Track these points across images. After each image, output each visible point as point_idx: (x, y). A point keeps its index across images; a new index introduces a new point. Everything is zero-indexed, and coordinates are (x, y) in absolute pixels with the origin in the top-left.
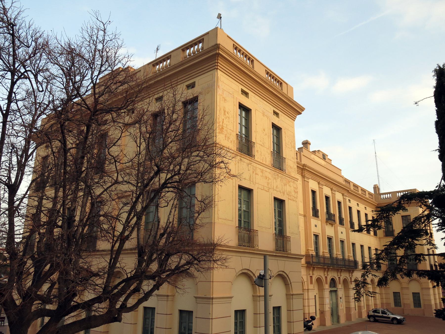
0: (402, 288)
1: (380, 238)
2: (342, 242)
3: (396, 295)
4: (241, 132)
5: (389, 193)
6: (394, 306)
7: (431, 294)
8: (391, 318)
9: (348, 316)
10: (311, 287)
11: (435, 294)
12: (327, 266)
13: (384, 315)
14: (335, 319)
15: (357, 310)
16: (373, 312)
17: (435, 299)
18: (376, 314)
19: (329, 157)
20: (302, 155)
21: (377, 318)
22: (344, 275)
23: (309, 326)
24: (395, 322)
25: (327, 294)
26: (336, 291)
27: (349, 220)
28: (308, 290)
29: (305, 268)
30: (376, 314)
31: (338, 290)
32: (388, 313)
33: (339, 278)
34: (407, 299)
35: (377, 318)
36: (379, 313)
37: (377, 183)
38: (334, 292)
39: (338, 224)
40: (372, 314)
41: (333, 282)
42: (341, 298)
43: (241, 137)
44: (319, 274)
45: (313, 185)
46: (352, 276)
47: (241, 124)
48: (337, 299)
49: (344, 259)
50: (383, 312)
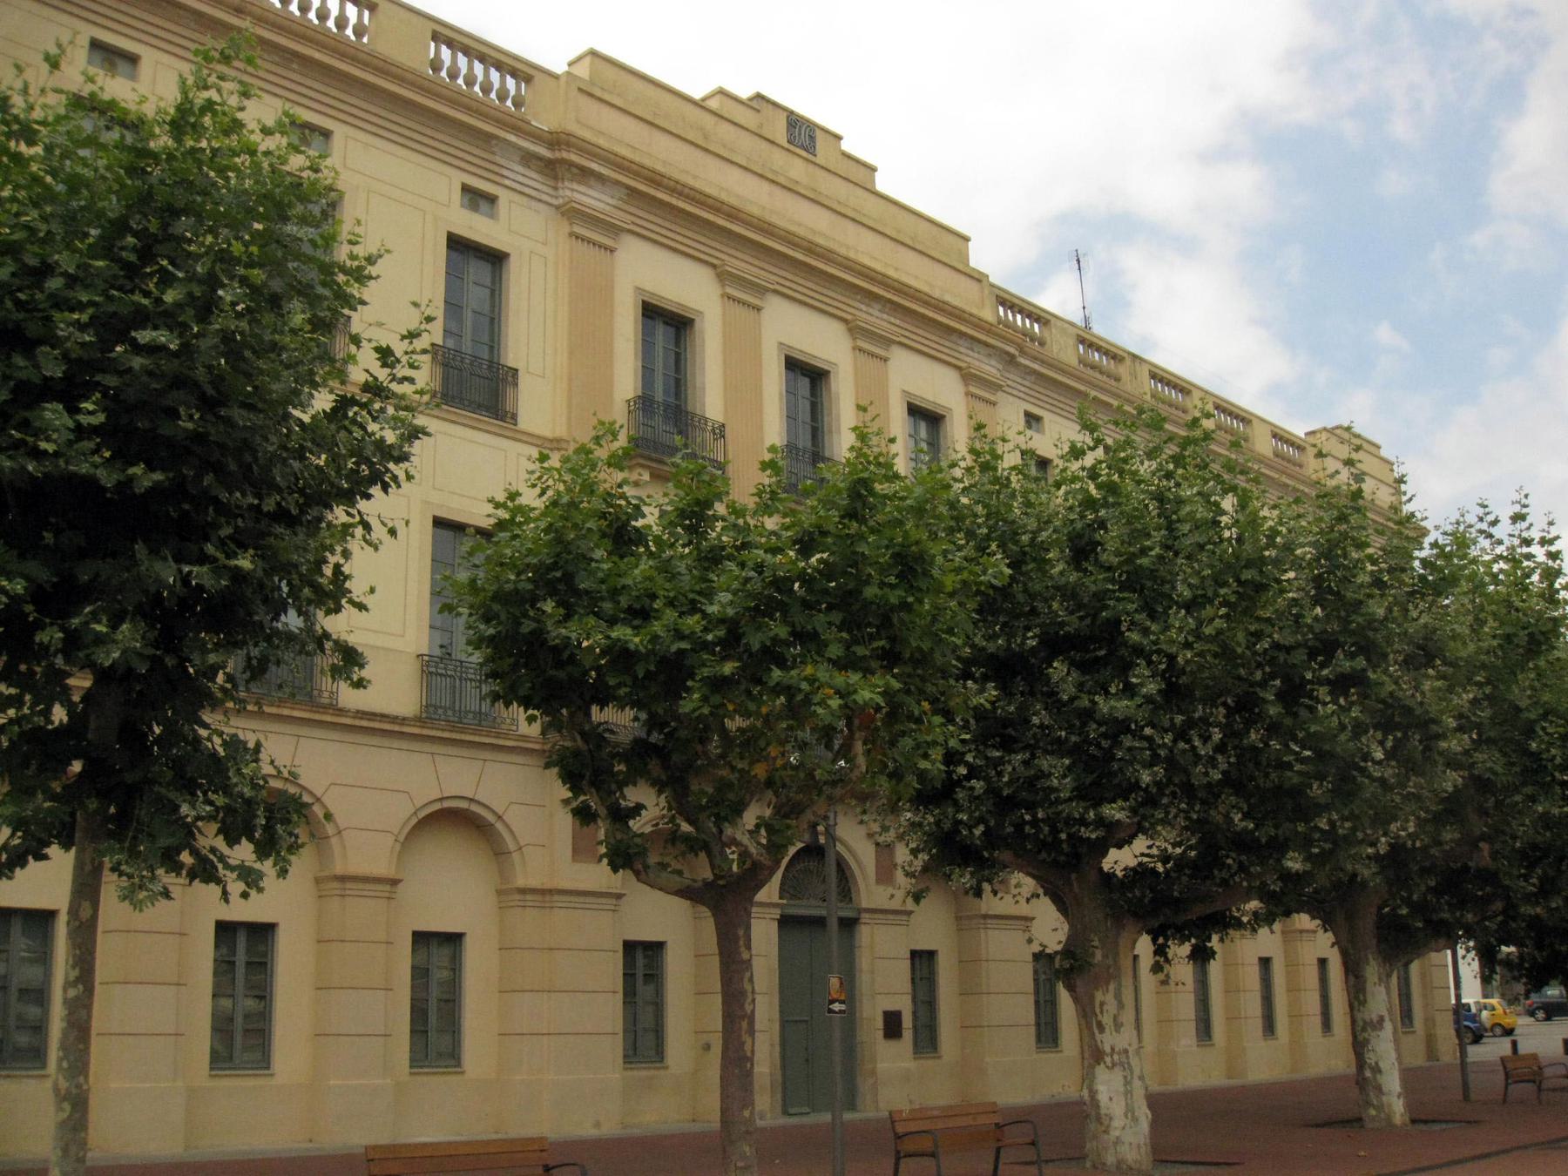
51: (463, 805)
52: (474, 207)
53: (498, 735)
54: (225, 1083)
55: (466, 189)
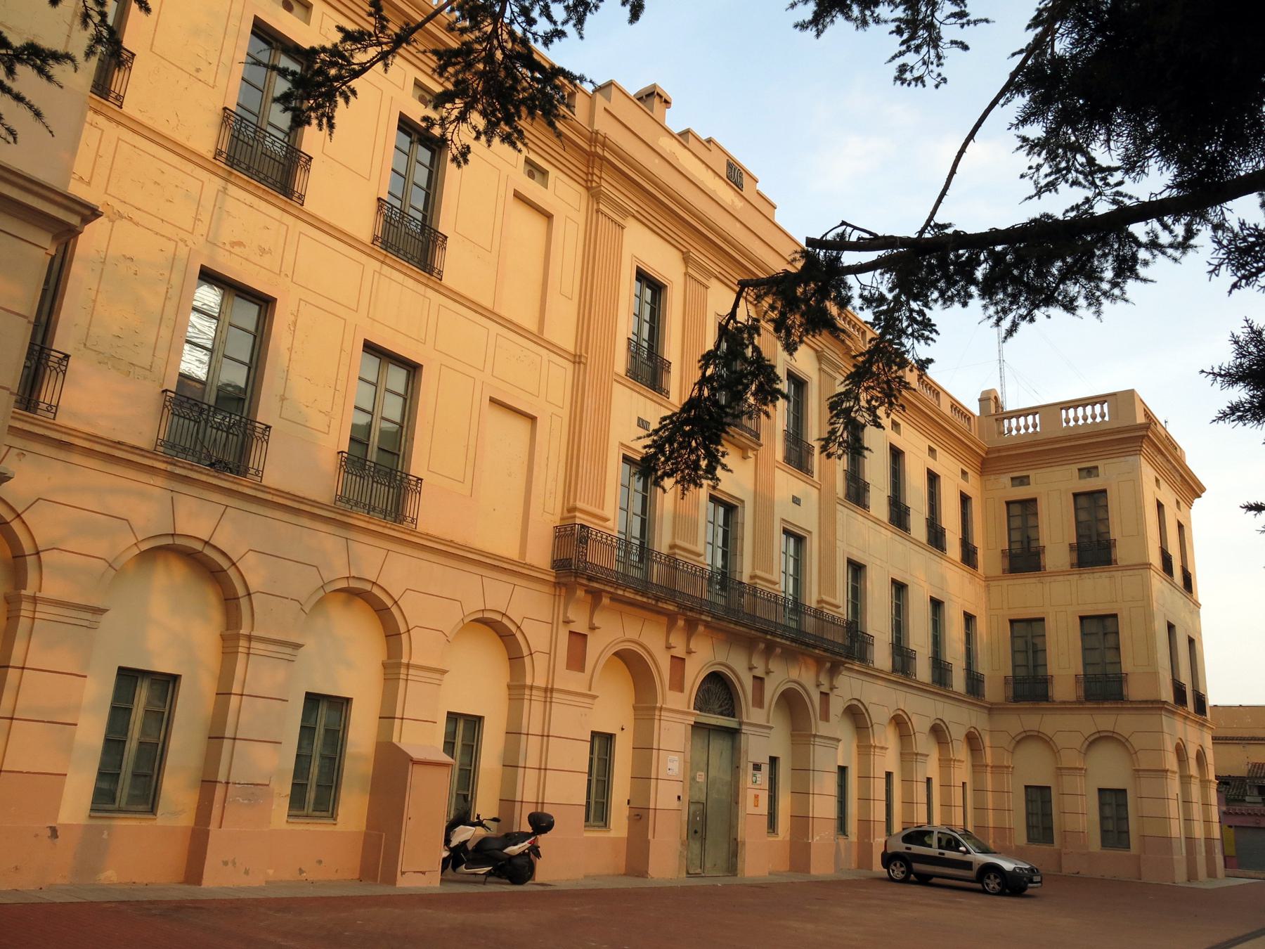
0: (1060, 771)
1: (987, 579)
3: (1039, 798)
4: (638, 334)
5: (1033, 411)
7: (1172, 795)
8: (976, 868)
9: (800, 851)
10: (568, 680)
12: (679, 606)
13: (949, 854)
17: (1188, 820)
18: (917, 849)
19: (759, 187)
21: (917, 867)
23: (511, 858)
24: (993, 884)
26: (733, 734)
30: (917, 849)
31: (745, 729)
32: (966, 845)
34: (1079, 814)
35: (917, 867)
36: (930, 846)
37: (993, 384)
39: (779, 454)
40: (900, 847)
41: (718, 690)
43: (638, 344)
47: (638, 316)
48: (735, 768)
49: (798, 607)
53: (911, 680)
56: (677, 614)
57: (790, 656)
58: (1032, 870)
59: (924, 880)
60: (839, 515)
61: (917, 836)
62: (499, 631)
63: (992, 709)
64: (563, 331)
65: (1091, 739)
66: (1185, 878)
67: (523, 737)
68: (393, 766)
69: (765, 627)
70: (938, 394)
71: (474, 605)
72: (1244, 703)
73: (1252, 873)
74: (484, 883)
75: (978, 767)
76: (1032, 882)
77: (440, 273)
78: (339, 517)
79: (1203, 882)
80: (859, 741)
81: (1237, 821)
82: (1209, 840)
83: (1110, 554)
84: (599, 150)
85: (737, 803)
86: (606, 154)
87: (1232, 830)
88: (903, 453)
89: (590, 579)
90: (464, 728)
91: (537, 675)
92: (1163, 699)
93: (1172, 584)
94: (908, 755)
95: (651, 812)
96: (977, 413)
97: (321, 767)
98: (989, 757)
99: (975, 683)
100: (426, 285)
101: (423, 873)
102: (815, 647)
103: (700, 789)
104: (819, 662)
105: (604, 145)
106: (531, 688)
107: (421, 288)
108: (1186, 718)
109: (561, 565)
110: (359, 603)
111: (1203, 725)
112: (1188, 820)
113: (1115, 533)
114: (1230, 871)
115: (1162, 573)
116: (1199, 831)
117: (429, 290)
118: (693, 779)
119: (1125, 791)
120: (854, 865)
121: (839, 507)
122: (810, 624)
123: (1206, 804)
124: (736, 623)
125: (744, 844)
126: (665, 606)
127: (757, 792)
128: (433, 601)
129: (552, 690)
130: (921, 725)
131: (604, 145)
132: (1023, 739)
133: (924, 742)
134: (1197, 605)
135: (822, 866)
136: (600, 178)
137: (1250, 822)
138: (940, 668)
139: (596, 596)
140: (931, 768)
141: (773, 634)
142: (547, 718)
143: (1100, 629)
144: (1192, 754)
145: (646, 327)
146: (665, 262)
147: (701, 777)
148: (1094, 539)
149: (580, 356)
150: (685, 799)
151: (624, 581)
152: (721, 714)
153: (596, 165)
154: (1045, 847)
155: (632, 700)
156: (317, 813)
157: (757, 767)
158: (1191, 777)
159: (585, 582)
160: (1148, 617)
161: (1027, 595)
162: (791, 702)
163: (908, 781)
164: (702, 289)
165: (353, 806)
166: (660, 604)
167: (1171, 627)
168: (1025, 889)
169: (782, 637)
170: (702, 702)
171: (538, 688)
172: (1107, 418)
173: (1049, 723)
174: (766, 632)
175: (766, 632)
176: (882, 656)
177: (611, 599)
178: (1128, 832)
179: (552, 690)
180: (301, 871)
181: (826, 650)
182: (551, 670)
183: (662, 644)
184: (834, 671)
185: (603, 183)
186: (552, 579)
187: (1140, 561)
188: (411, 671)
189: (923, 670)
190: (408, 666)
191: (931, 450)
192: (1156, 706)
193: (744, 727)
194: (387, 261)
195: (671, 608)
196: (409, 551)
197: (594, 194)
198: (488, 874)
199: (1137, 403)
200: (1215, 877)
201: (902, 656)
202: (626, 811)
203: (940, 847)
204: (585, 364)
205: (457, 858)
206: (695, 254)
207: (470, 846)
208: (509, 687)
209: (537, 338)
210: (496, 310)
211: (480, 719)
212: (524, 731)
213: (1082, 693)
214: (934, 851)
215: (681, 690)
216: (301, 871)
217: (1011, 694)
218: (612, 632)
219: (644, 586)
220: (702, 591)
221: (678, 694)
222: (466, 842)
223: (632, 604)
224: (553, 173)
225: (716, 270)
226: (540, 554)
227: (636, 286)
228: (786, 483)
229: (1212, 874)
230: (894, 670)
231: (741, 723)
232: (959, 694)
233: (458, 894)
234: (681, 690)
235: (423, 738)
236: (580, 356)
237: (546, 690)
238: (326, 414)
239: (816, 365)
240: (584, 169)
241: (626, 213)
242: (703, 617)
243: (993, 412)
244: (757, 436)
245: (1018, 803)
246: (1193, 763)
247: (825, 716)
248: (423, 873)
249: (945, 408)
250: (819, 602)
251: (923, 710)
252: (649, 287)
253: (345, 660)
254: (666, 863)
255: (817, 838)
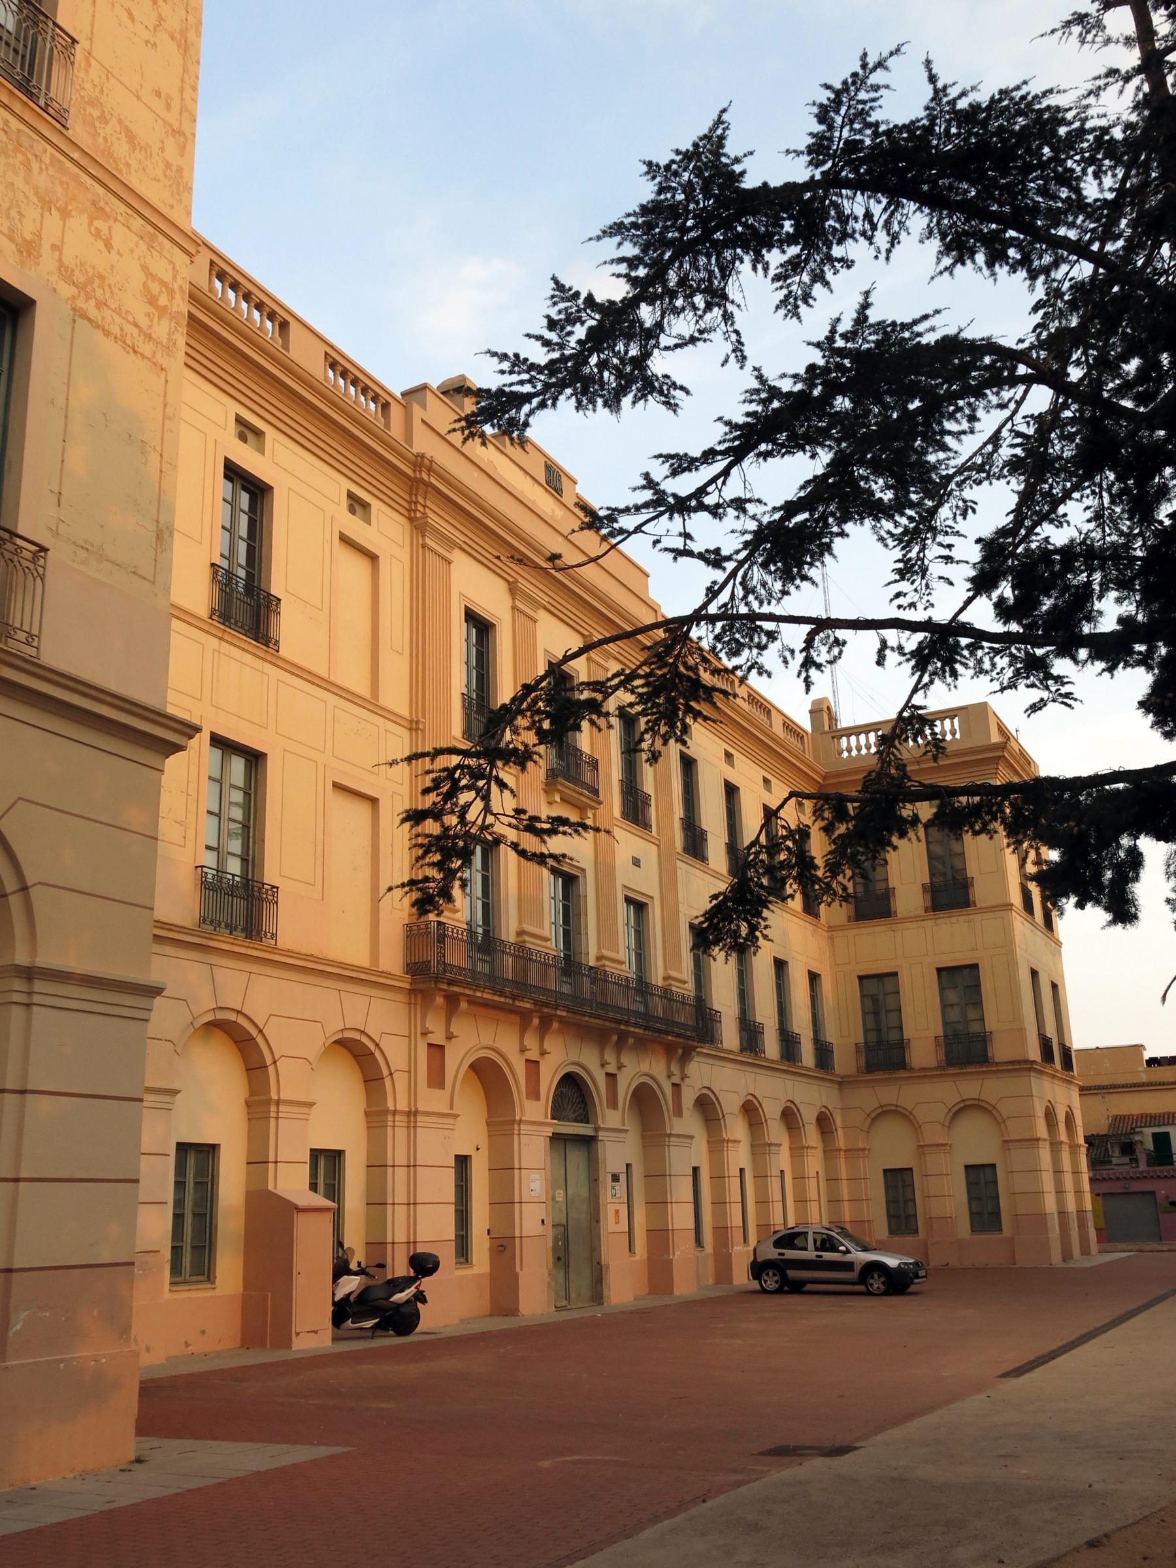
1: (831, 929)
2: (638, 907)
3: (898, 1182)
4: (230, 557)
6: (886, 1233)
8: (858, 1268)
9: (659, 1270)
10: (431, 1100)
11: (1058, 1172)
12: (536, 1002)
13: (828, 1256)
14: (581, 1282)
15: (709, 1248)
16: (778, 1244)
17: (1060, 1192)
18: (791, 1254)
19: (579, 489)
20: (417, 422)
21: (792, 1274)
22: (641, 1067)
23: (398, 1306)
24: (877, 1284)
25: (532, 1148)
26: (588, 1142)
27: (678, 811)
28: (412, 1114)
29: (402, 997)
30: (791, 1254)
33: (611, 1076)
34: (945, 1197)
35: (792, 1274)
36: (806, 1249)
38: (576, 1144)
40: (772, 1253)
41: (573, 1095)
42: (615, 1178)
43: (229, 573)
44: (487, 1040)
45: (476, 584)
46: (684, 1077)
47: (231, 530)
48: (594, 1181)
49: (642, 987)
50: (827, 1244)
51: (232, 1017)
52: (243, 438)
53: (718, 1049)
54: (984, 1237)
55: (240, 421)
56: (531, 1011)
57: (642, 1045)
58: (916, 1264)
59: (796, 1288)
60: (679, 872)
61: (788, 1240)
62: (356, 1052)
63: (842, 1084)
64: (395, 696)
65: (954, 1110)
66: (1060, 1259)
67: (390, 1170)
68: (271, 1218)
69: (618, 1016)
70: (769, 712)
71: (334, 1027)
72: (1101, 1045)
73: (1124, 1246)
74: (373, 1338)
75: (830, 1152)
76: (917, 1277)
77: (277, 643)
78: (204, 942)
79: (1079, 1261)
80: (709, 1135)
81: (1105, 1188)
82: (1081, 1212)
83: (967, 894)
84: (425, 477)
85: (598, 1221)
86: (433, 480)
87: (1100, 1198)
88: (738, 788)
89: (451, 983)
90: (327, 1165)
91: (398, 1098)
92: (1031, 1059)
93: (1033, 924)
94: (760, 1148)
95: (517, 1241)
96: (808, 728)
97: (193, 1225)
98: (841, 1140)
99: (824, 1053)
100: (264, 659)
101: (316, 1332)
102: (667, 1033)
103: (560, 1210)
104: (669, 1050)
105: (430, 470)
106: (394, 1113)
107: (258, 663)
108: (1053, 1077)
109: (416, 969)
110: (217, 1031)
111: (1070, 1082)
112: (1060, 1192)
113: (972, 871)
114: (1107, 1246)
115: (1024, 913)
116: (1071, 1207)
117: (267, 665)
118: (554, 1198)
119: (993, 1166)
120: (711, 1281)
121: (679, 863)
122: (658, 1007)
123: (1076, 1173)
124: (591, 1016)
125: (608, 1267)
126: (522, 1004)
127: (617, 1207)
128: (297, 1021)
129: (416, 1113)
130: (772, 1111)
131: (430, 470)
132: (879, 1115)
133: (776, 1132)
134: (1059, 944)
135: (685, 1286)
136: (424, 506)
137: (1117, 1187)
138: (789, 1042)
139: (452, 1001)
140: (782, 1160)
141: (627, 1023)
142: (412, 1145)
143: (961, 981)
144: (1061, 1117)
145: (242, 547)
146: (492, 598)
147: (560, 1196)
148: (949, 877)
149: (417, 722)
150: (549, 1222)
151: (473, 979)
152: (575, 1121)
153: (421, 492)
154: (909, 1238)
155: (483, 1114)
156: (194, 1278)
157: (615, 1178)
158: (1062, 1142)
159: (445, 987)
160: (1011, 962)
161: (876, 946)
162: (644, 1100)
163: (761, 1177)
164: (530, 623)
165: (229, 1265)
166: (517, 1003)
167: (1034, 973)
168: (908, 1286)
169: (636, 1025)
170: (558, 1111)
171: (401, 1112)
172: (958, 736)
173: (907, 1094)
174: (619, 1022)
175: (619, 1022)
176: (730, 1035)
177: (469, 1002)
178: (915, 1215)
179: (416, 1113)
180: (187, 1344)
181: (678, 1035)
182: (413, 1093)
183: (517, 1048)
184: (685, 1059)
185: (427, 511)
186: (407, 986)
187: (1000, 902)
188: (282, 1108)
189: (771, 1046)
190: (278, 1102)
191: (728, 756)
192: (1023, 1066)
193: (600, 1133)
194: (226, 637)
195: (528, 1005)
196: (269, 971)
197: (418, 526)
198: (376, 1327)
199: (990, 715)
200: (1089, 1254)
201: (750, 1032)
202: (486, 1244)
203: (817, 1249)
204: (423, 731)
205: (342, 1311)
206: (523, 584)
207: (352, 1298)
208: (367, 1114)
209: (371, 704)
210: (332, 679)
211: (214, 1148)
212: (390, 1163)
213: (942, 1057)
214: (811, 1254)
215: (538, 1098)
216: (187, 1344)
217: (863, 1062)
218: (471, 1039)
219: (494, 982)
220: (553, 982)
221: (535, 1103)
222: (351, 1293)
223: (487, 1005)
224: (375, 505)
225: (544, 599)
226: (392, 960)
227: (223, 488)
228: (627, 843)
229: (1086, 1251)
230: (743, 1050)
231: (597, 1129)
232: (809, 1069)
233: (396, 1346)
234: (538, 1098)
235: (292, 1182)
236: (417, 722)
237: (409, 1113)
238: (180, 823)
239: (507, 601)
240: (407, 497)
241: (451, 544)
242: (559, 1013)
243: (827, 728)
244: (596, 792)
245: (876, 1191)
246: (1062, 1126)
247: (679, 1112)
248: (316, 1332)
249: (778, 729)
250: (666, 979)
251: (774, 1091)
252: (245, 489)
253: (209, 1102)
254: (536, 1298)
255: (678, 1253)
